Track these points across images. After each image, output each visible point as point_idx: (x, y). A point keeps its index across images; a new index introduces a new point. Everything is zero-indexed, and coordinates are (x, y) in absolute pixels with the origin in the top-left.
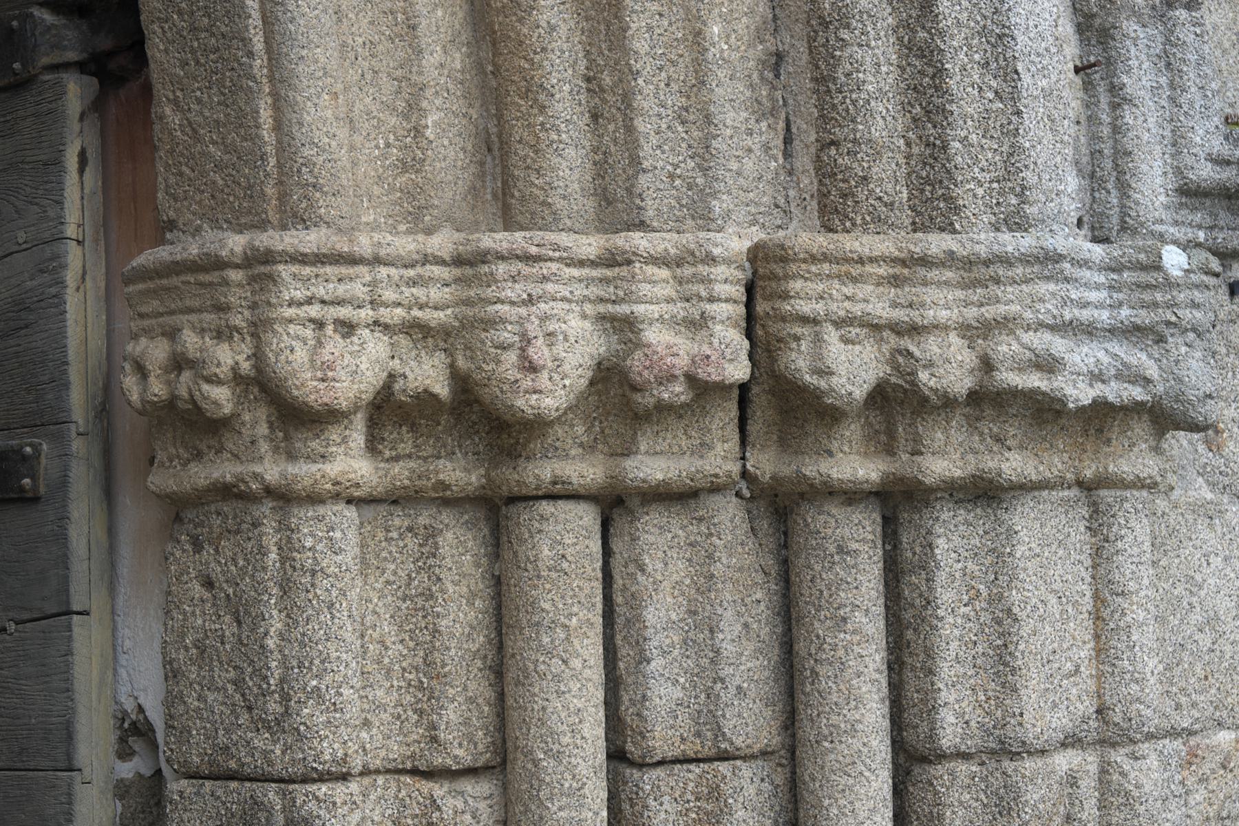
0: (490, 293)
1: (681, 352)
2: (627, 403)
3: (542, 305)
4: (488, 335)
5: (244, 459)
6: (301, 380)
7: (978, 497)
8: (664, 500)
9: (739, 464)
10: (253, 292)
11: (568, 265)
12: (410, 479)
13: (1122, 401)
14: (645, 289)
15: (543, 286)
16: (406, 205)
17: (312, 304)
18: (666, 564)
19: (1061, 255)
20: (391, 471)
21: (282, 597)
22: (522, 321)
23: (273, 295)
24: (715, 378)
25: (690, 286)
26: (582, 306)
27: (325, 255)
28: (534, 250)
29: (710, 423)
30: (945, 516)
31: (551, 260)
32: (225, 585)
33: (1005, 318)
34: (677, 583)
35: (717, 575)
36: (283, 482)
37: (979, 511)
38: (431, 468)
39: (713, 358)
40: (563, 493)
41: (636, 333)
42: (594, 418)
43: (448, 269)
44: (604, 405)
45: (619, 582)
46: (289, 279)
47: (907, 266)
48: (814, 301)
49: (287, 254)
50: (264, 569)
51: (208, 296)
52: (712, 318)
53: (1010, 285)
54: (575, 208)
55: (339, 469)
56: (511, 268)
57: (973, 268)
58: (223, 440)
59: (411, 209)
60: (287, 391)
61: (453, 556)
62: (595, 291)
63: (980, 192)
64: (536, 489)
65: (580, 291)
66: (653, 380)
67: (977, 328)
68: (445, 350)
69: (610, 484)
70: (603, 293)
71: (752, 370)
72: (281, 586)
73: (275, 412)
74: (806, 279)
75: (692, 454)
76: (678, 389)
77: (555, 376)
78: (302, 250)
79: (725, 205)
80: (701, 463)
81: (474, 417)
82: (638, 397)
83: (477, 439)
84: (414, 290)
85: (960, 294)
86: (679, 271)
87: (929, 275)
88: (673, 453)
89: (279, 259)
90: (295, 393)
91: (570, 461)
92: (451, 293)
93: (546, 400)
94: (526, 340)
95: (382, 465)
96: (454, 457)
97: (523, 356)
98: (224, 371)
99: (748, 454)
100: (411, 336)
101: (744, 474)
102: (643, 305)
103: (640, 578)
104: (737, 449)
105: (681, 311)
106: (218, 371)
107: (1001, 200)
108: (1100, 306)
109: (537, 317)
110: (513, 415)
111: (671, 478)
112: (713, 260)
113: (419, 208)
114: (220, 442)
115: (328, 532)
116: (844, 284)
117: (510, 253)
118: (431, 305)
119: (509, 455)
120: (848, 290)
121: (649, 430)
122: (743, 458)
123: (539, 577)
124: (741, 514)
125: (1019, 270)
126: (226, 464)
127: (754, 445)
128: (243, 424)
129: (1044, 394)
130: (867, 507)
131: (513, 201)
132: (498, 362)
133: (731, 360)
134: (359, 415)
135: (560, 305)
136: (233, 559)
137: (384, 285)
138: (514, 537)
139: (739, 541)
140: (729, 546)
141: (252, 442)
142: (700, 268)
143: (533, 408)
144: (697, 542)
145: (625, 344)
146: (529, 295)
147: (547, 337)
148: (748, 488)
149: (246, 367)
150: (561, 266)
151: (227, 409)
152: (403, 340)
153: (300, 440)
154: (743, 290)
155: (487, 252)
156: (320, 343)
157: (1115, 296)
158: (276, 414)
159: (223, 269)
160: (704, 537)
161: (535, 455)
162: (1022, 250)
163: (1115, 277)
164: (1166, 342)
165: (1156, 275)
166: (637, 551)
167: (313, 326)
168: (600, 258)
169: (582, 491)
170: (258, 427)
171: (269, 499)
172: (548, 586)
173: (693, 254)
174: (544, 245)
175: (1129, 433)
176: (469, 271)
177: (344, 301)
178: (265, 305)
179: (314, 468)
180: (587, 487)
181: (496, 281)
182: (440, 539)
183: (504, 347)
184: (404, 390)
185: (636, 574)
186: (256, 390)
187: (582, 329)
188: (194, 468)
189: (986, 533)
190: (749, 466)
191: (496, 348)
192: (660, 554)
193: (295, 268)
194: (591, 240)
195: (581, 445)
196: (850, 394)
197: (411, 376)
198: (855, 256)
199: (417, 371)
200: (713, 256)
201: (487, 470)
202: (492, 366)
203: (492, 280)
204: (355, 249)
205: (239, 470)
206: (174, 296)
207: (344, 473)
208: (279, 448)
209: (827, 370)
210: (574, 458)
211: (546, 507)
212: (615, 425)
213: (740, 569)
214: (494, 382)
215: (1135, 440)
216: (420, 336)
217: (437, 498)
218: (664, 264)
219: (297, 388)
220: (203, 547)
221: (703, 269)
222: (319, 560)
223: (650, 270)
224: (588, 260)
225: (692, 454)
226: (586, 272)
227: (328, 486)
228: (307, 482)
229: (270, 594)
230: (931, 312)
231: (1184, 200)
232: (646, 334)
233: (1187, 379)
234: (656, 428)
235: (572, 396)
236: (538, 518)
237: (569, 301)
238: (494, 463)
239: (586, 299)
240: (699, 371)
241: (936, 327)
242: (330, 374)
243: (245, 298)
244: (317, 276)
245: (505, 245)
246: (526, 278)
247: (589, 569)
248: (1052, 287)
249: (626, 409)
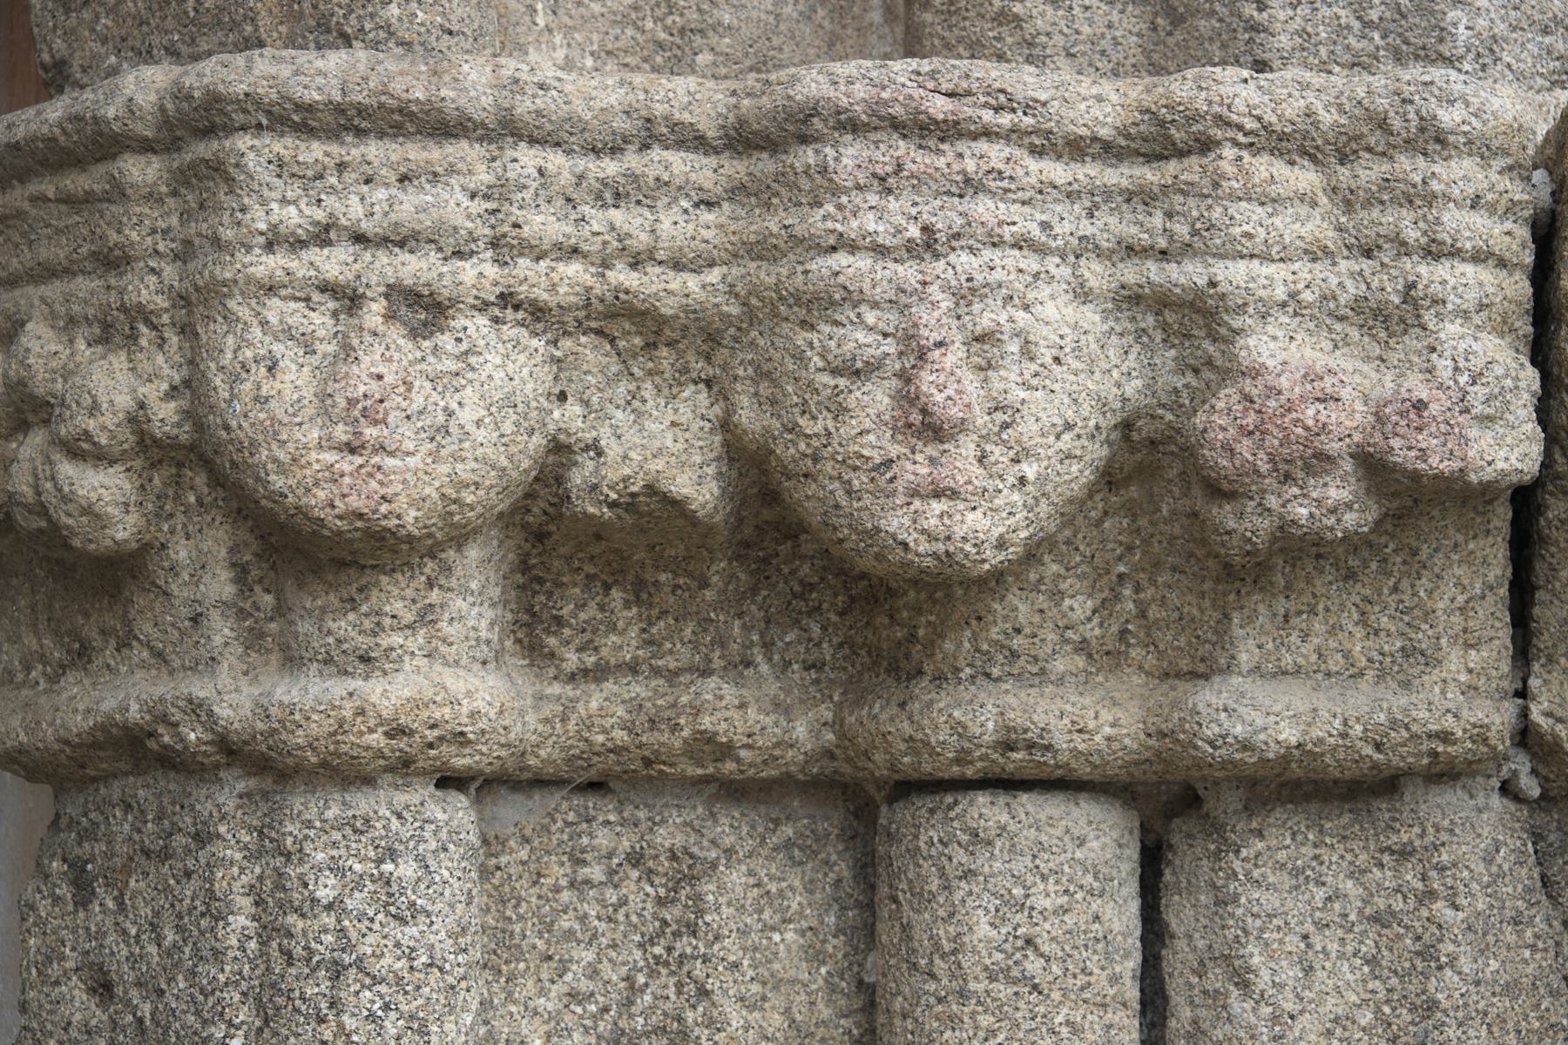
0: (818, 221)
1: (1345, 393)
2: (1198, 532)
3: (963, 259)
4: (814, 337)
5: (177, 663)
6: (291, 447)
8: (1307, 798)
9: (1510, 708)
10: (186, 215)
11: (1037, 152)
12: (628, 728)
14: (1249, 218)
15: (966, 205)
16: (649, 25)
17: (327, 243)
18: (1309, 970)
20: (580, 707)
21: (260, 1030)
22: (904, 299)
23: (226, 219)
24: (1438, 463)
25: (1375, 213)
26: (1075, 266)
27: (361, 110)
28: (939, 107)
29: (1430, 593)
31: (988, 133)
32: (134, 994)
34: (1336, 1020)
35: (1445, 1004)
36: (260, 726)
38: (684, 699)
39: (1434, 408)
40: (1030, 773)
41: (1226, 341)
42: (1121, 576)
43: (712, 161)
44: (1146, 542)
45: (1182, 1014)
46: (265, 175)
49: (258, 103)
50: (218, 955)
51: (85, 231)
52: (1435, 302)
54: (1086, 30)
55: (407, 693)
56: (878, 156)
58: (132, 613)
59: (663, 36)
60: (258, 479)
61: (744, 932)
62: (1113, 225)
64: (958, 761)
65: (1069, 223)
66: (1264, 467)
68: (709, 383)
69: (1158, 754)
70: (1134, 230)
71: (1548, 452)
72: (260, 1006)
73: (251, 539)
75: (1380, 678)
76: (1336, 493)
77: (996, 452)
78: (299, 93)
79: (1482, 23)
80: (1404, 701)
81: (805, 569)
82: (1225, 515)
83: (816, 630)
84: (617, 216)
86: (1344, 173)
88: (1328, 675)
89: (239, 118)
90: (278, 482)
91: (1049, 689)
92: (720, 226)
93: (970, 516)
94: (916, 351)
95: (556, 689)
96: (750, 672)
97: (908, 397)
98: (105, 426)
99: (1534, 683)
100: (612, 341)
101: (1525, 735)
102: (1242, 265)
103: (1238, 1005)
104: (1505, 666)
105: (1349, 283)
106: (91, 424)
109: (946, 288)
110: (879, 557)
111: (1321, 741)
112: (1440, 140)
113: (682, 31)
114: (127, 622)
115: (379, 862)
117: (874, 114)
118: (661, 255)
119: (894, 669)
121: (1262, 609)
122: (1522, 693)
123: (963, 995)
124: (1514, 842)
126: (139, 674)
127: (1551, 660)
128: (173, 570)
131: (928, 17)
132: (840, 412)
133: (1486, 420)
134: (473, 553)
135: (1013, 258)
136: (154, 927)
137: (528, 195)
138: (904, 886)
139: (1508, 913)
140: (1479, 927)
141: (195, 620)
142: (1404, 162)
143: (931, 537)
144: (1393, 914)
145: (1196, 371)
146: (925, 229)
147: (976, 347)
148: (1534, 772)
149: (165, 415)
150: (1017, 152)
151: (124, 529)
152: (590, 353)
153: (310, 612)
154: (1524, 233)
155: (811, 111)
156: (347, 352)
158: (255, 546)
159: (114, 157)
160: (1412, 901)
161: (957, 670)
166: (1230, 933)
167: (332, 305)
168: (1128, 136)
169: (1084, 771)
170: (207, 578)
171: (237, 772)
172: (986, 1020)
173: (1383, 124)
174: (969, 93)
176: (765, 165)
177: (415, 236)
178: (208, 249)
179: (338, 688)
180: (1096, 759)
181: (836, 191)
182: (708, 888)
183: (856, 371)
184: (595, 487)
185: (1227, 995)
186: (201, 480)
187: (1076, 326)
188: (73, 687)
190: (1536, 715)
191: (835, 372)
192: (1293, 943)
193: (282, 146)
194: (1107, 88)
195: (1083, 647)
197: (613, 449)
199: (632, 437)
200: (1439, 130)
201: (839, 707)
202: (824, 422)
203: (825, 186)
204: (444, 92)
205: (159, 691)
206: (17, 238)
207: (418, 704)
208: (262, 635)
210: (1060, 681)
211: (986, 810)
212: (1173, 598)
213: (1510, 989)
214: (829, 467)
216: (638, 341)
217: (706, 780)
218: (1304, 153)
219: (282, 469)
220: (93, 893)
221: (1410, 167)
222: (353, 935)
223: (1263, 167)
224: (1095, 139)
225: (1380, 678)
226: (1088, 172)
227: (377, 739)
228: (319, 727)
229: (230, 1024)
232: (1252, 342)
234: (1281, 606)
235: (1044, 508)
236: (965, 838)
237: (1041, 250)
238: (856, 693)
239: (1086, 247)
240: (1396, 443)
242: (370, 432)
243: (165, 232)
244: (341, 167)
245: (860, 91)
246: (919, 182)
247: (1100, 978)
249: (1200, 553)
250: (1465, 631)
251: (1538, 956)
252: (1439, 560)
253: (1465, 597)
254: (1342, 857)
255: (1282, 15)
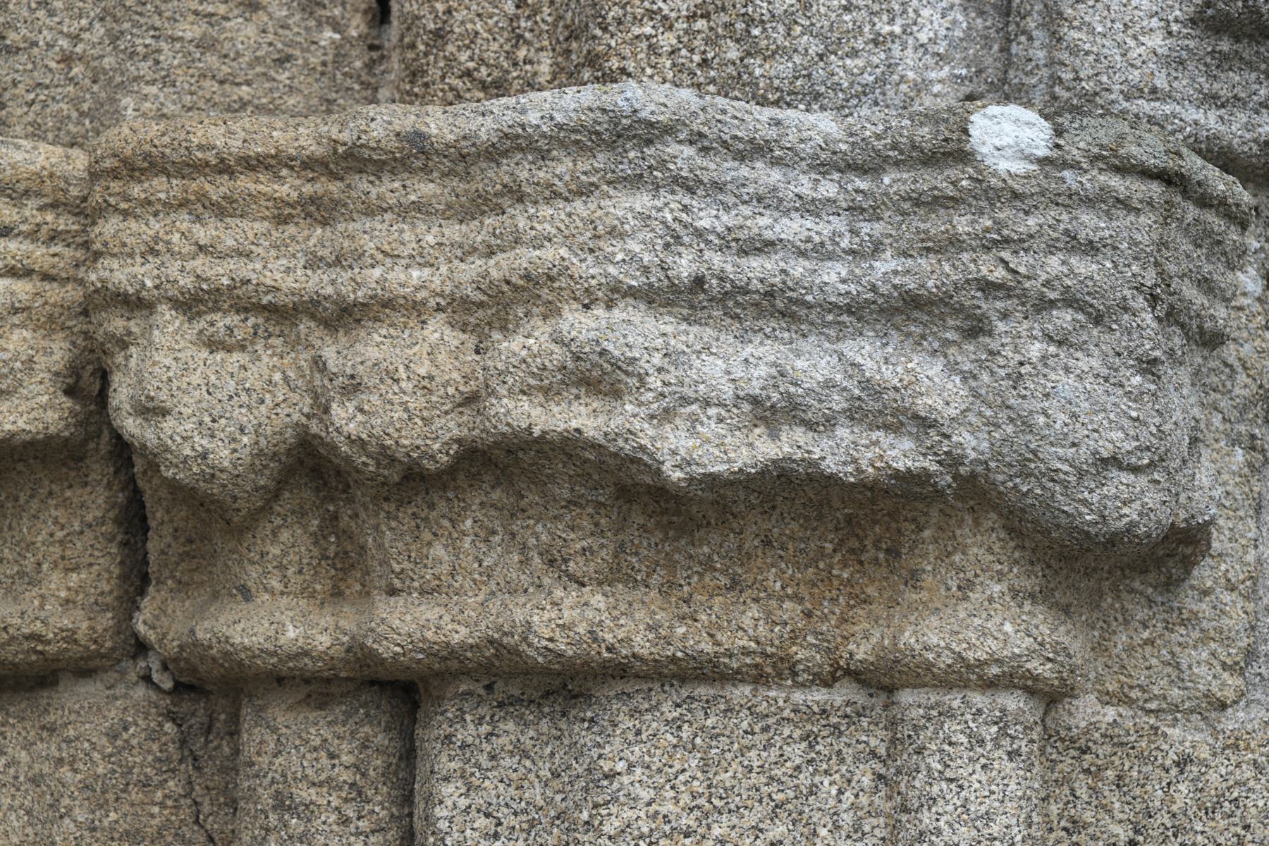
7: (547, 694)
13: (859, 471)
19: (651, 125)
30: (467, 733)
33: (527, 277)
37: (544, 725)
47: (335, 176)
48: (139, 260)
53: (547, 201)
57: (473, 169)
63: (667, 40)
67: (481, 305)
74: (125, 214)
85: (454, 231)
87: (374, 191)
107: (710, 56)
108: (819, 251)
116: (198, 219)
120: (203, 234)
125: (564, 167)
129: (594, 446)
130: (348, 715)
157: (865, 228)
162: (559, 118)
163: (863, 185)
164: (990, 334)
165: (953, 173)
175: (957, 558)
189: (556, 775)
196: (204, 456)
198: (211, 157)
209: (150, 405)
215: (970, 575)
230: (377, 272)
231: (1225, 46)
233: (1042, 420)
241: (388, 304)
248: (643, 201)
250: (63, 558)
251: (166, 812)
252: (35, 504)
253: (65, 532)
254: (19, 733)
255: (19, 112)
